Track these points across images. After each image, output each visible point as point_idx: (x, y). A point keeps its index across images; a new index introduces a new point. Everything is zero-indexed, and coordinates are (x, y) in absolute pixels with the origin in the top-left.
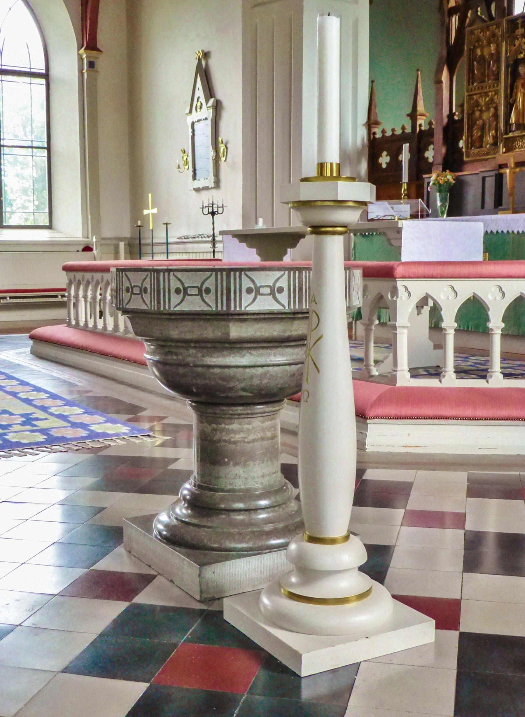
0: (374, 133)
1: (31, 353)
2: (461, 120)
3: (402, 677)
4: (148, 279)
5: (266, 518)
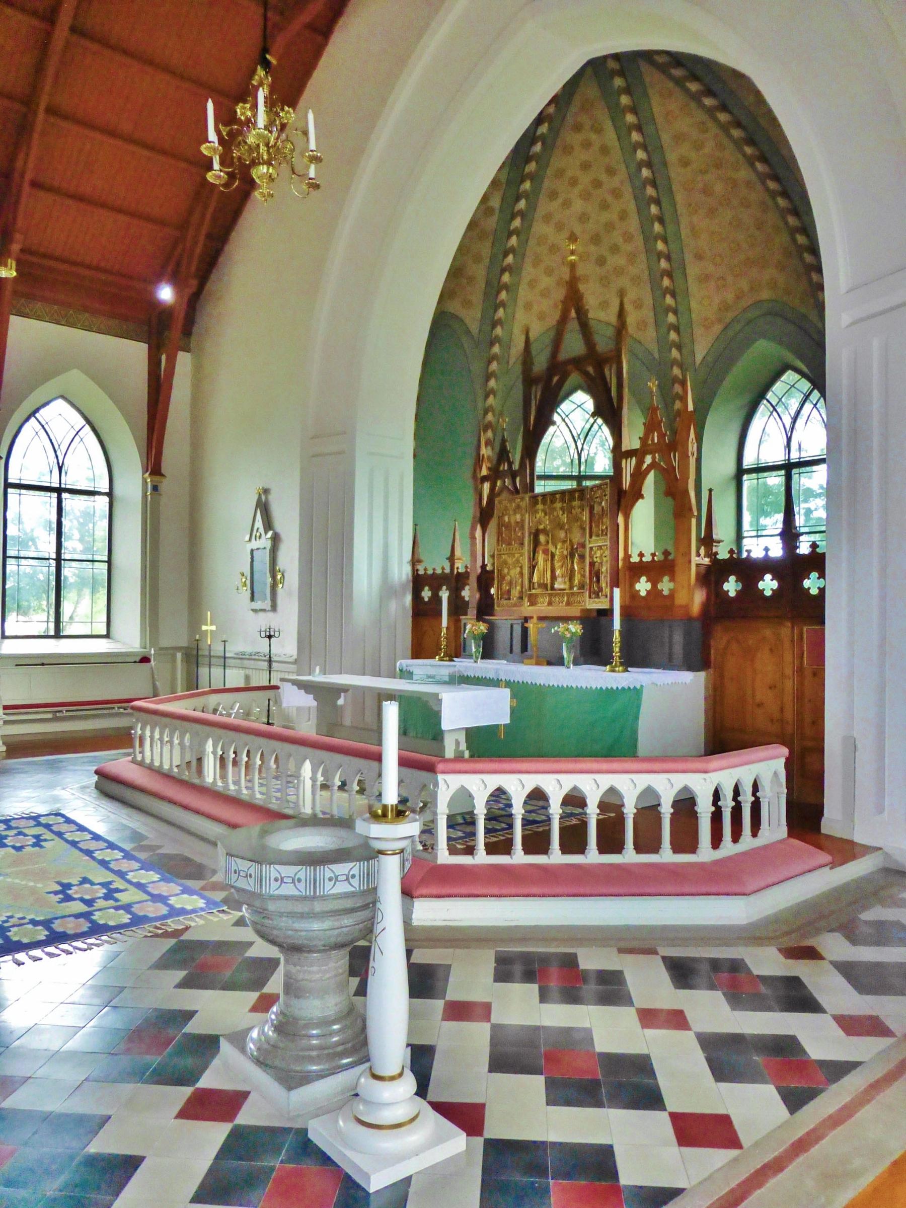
0: (417, 570)
1: (96, 787)
2: (493, 572)
3: (442, 1177)
4: (253, 868)
5: (342, 1059)
